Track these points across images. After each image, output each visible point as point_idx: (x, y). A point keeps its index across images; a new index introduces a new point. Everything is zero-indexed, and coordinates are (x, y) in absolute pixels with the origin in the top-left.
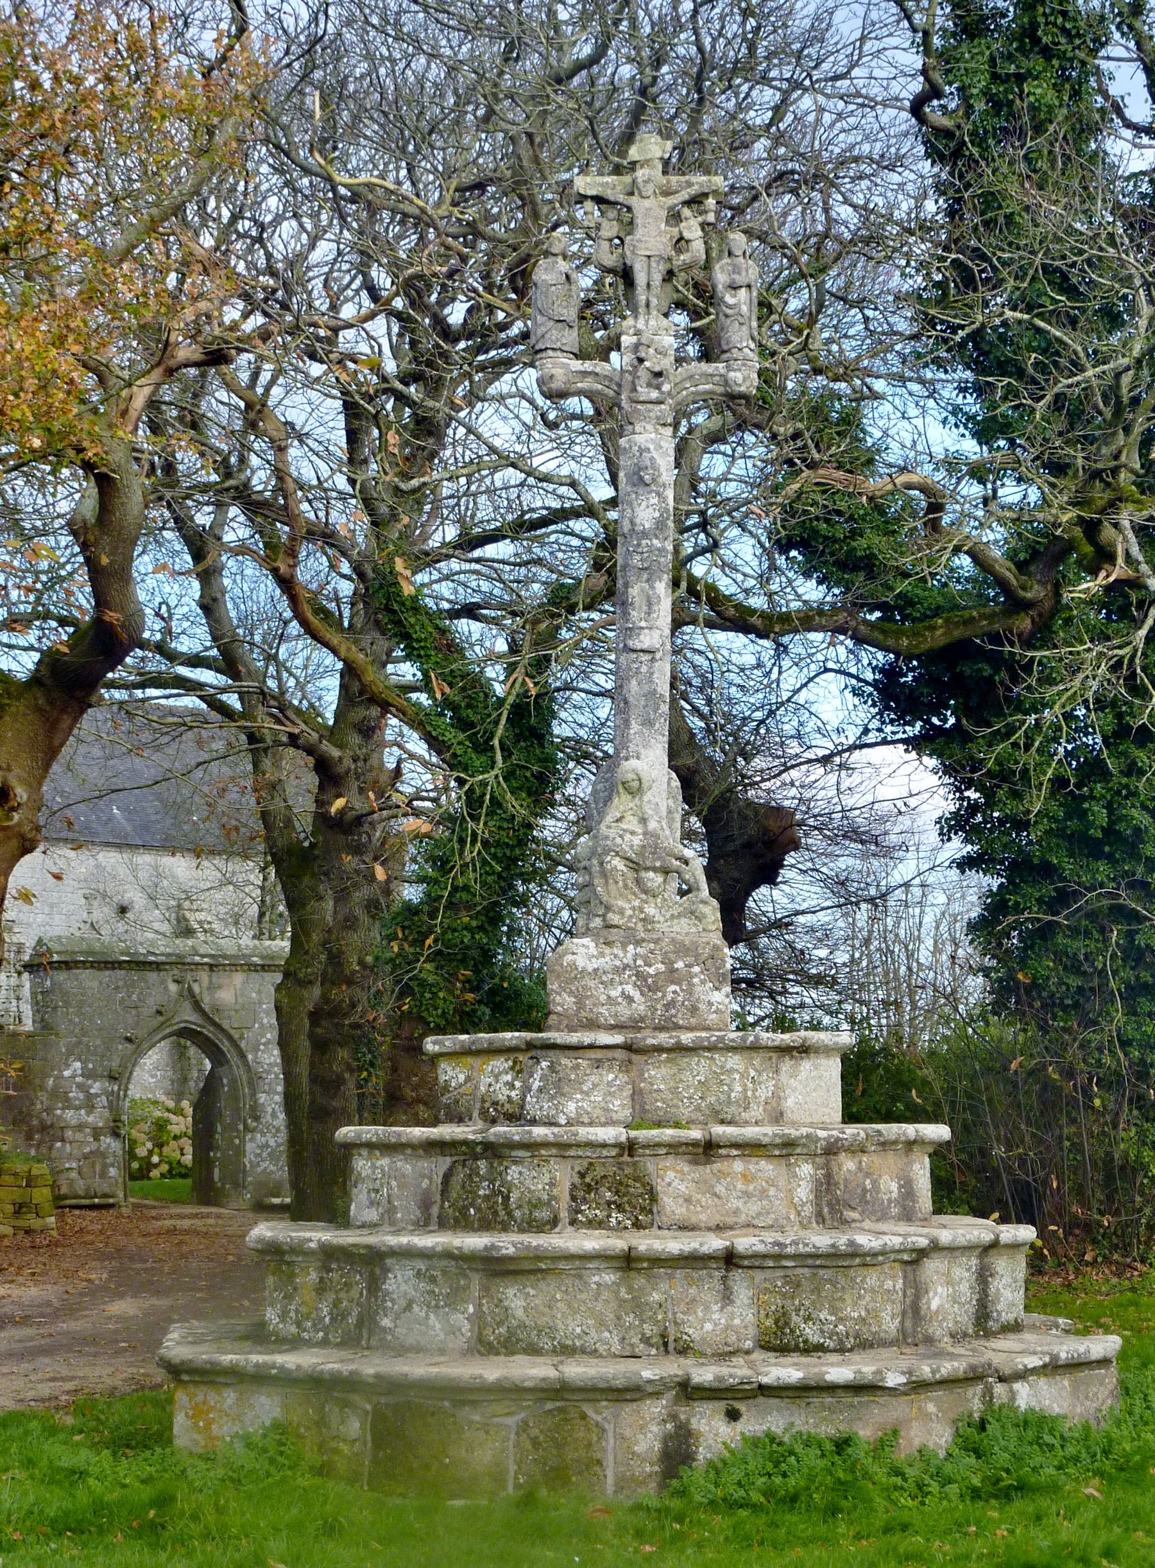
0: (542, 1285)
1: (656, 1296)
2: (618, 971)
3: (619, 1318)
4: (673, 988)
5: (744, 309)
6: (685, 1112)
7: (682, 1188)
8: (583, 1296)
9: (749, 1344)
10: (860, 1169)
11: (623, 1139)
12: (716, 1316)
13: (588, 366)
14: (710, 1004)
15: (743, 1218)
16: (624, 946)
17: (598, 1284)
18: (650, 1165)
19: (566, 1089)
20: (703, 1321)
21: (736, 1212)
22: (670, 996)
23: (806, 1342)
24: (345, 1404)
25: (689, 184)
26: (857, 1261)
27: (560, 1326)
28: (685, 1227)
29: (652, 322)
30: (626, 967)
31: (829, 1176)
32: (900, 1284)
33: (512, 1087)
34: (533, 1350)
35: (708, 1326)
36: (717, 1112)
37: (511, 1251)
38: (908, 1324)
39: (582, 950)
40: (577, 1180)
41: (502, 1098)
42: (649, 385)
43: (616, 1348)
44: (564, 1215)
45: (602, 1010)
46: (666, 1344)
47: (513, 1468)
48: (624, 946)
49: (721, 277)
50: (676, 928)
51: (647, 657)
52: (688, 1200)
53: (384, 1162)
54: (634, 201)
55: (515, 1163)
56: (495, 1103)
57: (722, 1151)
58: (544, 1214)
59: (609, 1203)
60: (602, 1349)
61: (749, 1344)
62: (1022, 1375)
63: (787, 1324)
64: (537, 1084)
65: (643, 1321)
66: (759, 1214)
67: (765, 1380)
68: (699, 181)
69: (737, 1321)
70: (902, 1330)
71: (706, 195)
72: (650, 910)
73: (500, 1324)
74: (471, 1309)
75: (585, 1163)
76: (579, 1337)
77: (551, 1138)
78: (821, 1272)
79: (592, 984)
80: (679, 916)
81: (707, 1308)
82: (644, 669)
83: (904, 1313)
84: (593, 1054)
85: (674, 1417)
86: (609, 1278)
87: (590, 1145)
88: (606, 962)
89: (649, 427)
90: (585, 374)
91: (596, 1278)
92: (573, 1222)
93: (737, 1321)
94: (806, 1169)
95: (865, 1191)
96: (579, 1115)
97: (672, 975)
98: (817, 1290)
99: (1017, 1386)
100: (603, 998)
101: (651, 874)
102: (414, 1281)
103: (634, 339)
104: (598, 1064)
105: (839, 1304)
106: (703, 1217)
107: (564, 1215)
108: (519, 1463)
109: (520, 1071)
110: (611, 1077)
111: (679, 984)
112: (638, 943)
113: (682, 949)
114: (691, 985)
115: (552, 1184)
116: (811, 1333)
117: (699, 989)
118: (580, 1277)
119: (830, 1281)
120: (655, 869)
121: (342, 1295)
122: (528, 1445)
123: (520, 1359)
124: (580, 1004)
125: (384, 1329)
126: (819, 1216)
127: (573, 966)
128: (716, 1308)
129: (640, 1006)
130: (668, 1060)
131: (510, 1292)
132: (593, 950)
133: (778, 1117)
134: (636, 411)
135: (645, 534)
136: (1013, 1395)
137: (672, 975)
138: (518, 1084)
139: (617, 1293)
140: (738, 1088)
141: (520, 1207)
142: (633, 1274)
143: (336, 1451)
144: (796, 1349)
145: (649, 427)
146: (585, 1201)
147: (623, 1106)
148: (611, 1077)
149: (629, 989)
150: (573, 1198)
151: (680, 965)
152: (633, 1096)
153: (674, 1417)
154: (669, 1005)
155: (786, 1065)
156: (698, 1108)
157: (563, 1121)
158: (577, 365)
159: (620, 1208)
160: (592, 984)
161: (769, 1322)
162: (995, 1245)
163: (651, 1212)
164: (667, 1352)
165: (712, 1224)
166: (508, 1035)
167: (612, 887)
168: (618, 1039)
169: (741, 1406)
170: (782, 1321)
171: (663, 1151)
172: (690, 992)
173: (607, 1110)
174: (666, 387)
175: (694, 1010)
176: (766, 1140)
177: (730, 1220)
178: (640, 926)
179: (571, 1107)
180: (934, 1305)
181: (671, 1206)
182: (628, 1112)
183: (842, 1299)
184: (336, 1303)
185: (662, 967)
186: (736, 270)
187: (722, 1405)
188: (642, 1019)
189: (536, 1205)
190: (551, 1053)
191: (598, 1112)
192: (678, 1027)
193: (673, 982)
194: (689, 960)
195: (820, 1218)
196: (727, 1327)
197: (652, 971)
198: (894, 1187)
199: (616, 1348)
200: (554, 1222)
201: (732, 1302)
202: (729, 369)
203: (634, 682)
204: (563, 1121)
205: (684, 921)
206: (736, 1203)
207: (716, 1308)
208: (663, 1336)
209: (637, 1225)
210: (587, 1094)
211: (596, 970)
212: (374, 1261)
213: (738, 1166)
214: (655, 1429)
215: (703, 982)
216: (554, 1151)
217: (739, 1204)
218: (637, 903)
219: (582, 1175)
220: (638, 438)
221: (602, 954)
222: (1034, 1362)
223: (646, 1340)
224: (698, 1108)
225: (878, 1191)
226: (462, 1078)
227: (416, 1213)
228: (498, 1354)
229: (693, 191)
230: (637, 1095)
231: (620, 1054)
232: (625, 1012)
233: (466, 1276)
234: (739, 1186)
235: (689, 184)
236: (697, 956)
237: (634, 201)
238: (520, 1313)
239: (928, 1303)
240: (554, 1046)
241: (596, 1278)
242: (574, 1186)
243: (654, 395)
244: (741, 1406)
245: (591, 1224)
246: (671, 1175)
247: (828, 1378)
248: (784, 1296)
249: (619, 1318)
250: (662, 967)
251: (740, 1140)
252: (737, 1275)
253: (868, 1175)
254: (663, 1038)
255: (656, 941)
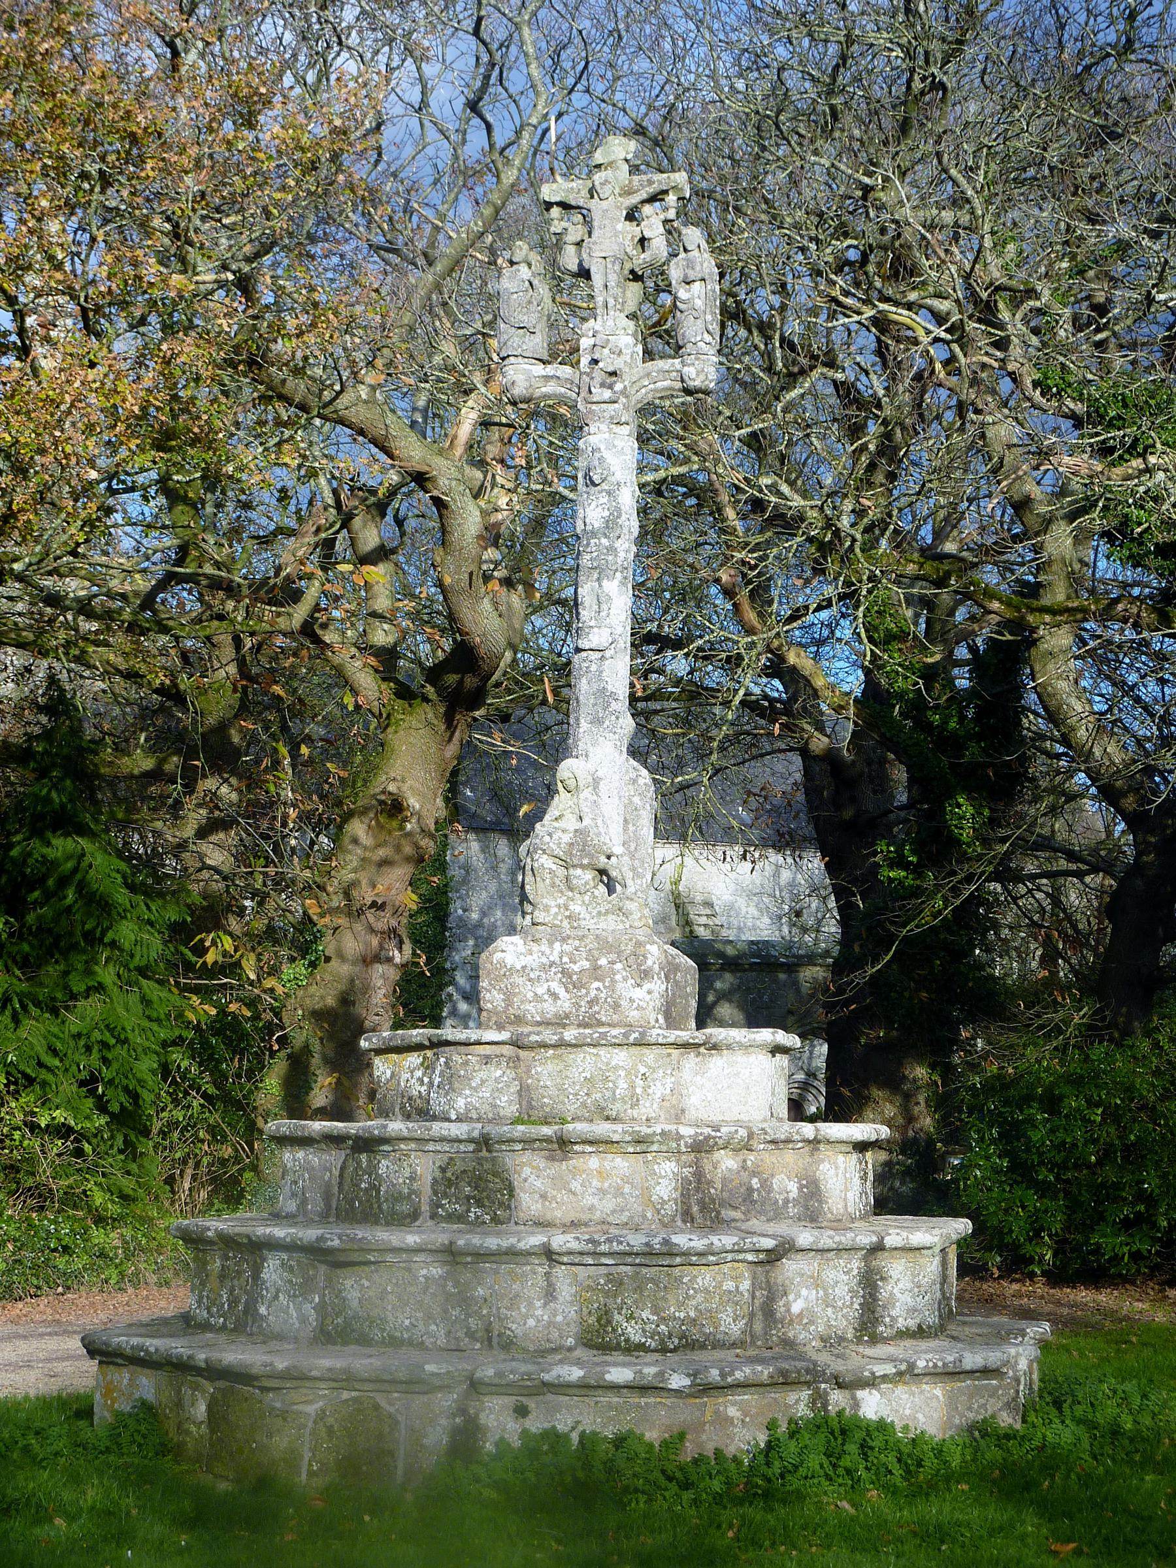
0: (376, 1277)
1: (480, 1291)
2: (544, 968)
3: (446, 1311)
4: (596, 984)
5: (699, 303)
6: (571, 1108)
7: (538, 1184)
8: (412, 1289)
9: (571, 1341)
10: (744, 1168)
11: (476, 1134)
12: (539, 1312)
13: (550, 370)
14: (632, 1000)
15: (597, 1215)
16: (551, 943)
17: (426, 1278)
18: (509, 1160)
19: (456, 1085)
20: (526, 1317)
21: (592, 1208)
22: (593, 993)
23: (627, 1341)
24: (196, 1387)
25: (650, 182)
26: (678, 1260)
27: (390, 1317)
28: (541, 1224)
29: (610, 323)
30: (552, 964)
31: (699, 1175)
32: (746, 1285)
33: (422, 1083)
34: (364, 1340)
35: (531, 1322)
36: (603, 1109)
37: (336, 1243)
38: (758, 1327)
39: (511, 948)
40: (438, 1174)
41: (415, 1093)
42: (602, 385)
43: (442, 1341)
44: (425, 1208)
45: (530, 1007)
46: (490, 1339)
47: (307, 1455)
48: (551, 943)
49: (675, 273)
50: (602, 926)
51: (598, 655)
52: (544, 1197)
53: (300, 1154)
54: (594, 204)
55: (385, 1157)
56: (410, 1098)
57: (577, 1148)
58: (405, 1208)
59: (468, 1198)
60: (428, 1342)
61: (571, 1341)
62: (871, 1382)
63: (609, 1322)
64: (437, 1080)
65: (468, 1315)
66: (614, 1211)
67: (546, 1377)
68: (660, 180)
69: (559, 1318)
70: (749, 1329)
71: (666, 192)
72: (576, 907)
73: (337, 1315)
74: (317, 1300)
75: (445, 1157)
76: (407, 1329)
77: (405, 1133)
78: (644, 1270)
79: (520, 981)
80: (607, 912)
81: (530, 1304)
82: (594, 668)
83: (752, 1315)
84: (480, 1049)
85: (463, 1411)
86: (436, 1271)
87: (442, 1139)
88: (532, 961)
89: (604, 427)
90: (547, 378)
91: (424, 1272)
92: (434, 1216)
93: (559, 1318)
94: (668, 1167)
95: (750, 1190)
96: (468, 1110)
97: (596, 972)
98: (639, 1289)
99: (860, 1394)
100: (530, 995)
101: (579, 871)
102: (280, 1271)
103: (592, 341)
104: (487, 1060)
105: (661, 1304)
106: (558, 1214)
107: (425, 1208)
108: (313, 1451)
109: (427, 1068)
110: (499, 1073)
111: (603, 981)
112: (564, 940)
113: (606, 945)
114: (613, 981)
115: (412, 1178)
116: (633, 1332)
117: (620, 986)
118: (409, 1270)
119: (652, 1280)
120: (582, 867)
121: (236, 1282)
122: (323, 1433)
123: (879, 1346)
124: (508, 1001)
125: (262, 1316)
126: (687, 1216)
127: (503, 963)
128: (538, 1304)
129: (565, 1003)
130: (554, 1057)
131: (348, 1283)
132: (521, 948)
133: (679, 1115)
134: (591, 412)
135: (593, 534)
136: (856, 1405)
137: (596, 972)
138: (426, 1080)
139: (445, 1286)
140: (622, 1084)
141: (386, 1200)
142: (460, 1268)
143: (188, 1432)
144: (618, 1347)
145: (604, 427)
146: (445, 1195)
147: (510, 1102)
148: (499, 1073)
149: (555, 986)
150: (435, 1193)
151: (603, 962)
152: (519, 1092)
153: (463, 1411)
154: (591, 1003)
155: (691, 1061)
156: (584, 1104)
157: (454, 1117)
158: (539, 370)
159: (479, 1203)
160: (520, 981)
161: (592, 1320)
162: (878, 1248)
163: (509, 1207)
164: (490, 1346)
165: (567, 1220)
166: (415, 1032)
167: (540, 884)
168: (504, 1036)
169: (531, 1403)
170: (605, 1318)
171: (519, 1147)
172: (612, 988)
173: (495, 1106)
174: (618, 387)
175: (616, 1006)
176: (616, 1138)
177: (585, 1217)
178: (565, 923)
179: (461, 1103)
180: (796, 1308)
181: (528, 1203)
182: (515, 1108)
183: (664, 1299)
184: (232, 1290)
185: (587, 965)
186: (690, 264)
187: (510, 1401)
188: (567, 1016)
189: (398, 1198)
190: (447, 1049)
191: (486, 1107)
192: (601, 1024)
193: (597, 979)
194: (613, 956)
195: (687, 1216)
196: (551, 1323)
197: (576, 968)
198: (793, 1188)
199: (442, 1341)
200: (415, 1215)
201: (555, 1298)
202: (683, 364)
203: (584, 681)
204: (454, 1117)
205: (611, 917)
206: (589, 1200)
207: (538, 1304)
208: (488, 1330)
209: (496, 1220)
210: (475, 1089)
211: (524, 968)
212: (257, 1248)
213: (594, 1162)
214: (444, 1422)
215: (625, 979)
216: (413, 1146)
217: (595, 1201)
218: (561, 901)
219: (443, 1170)
220: (592, 439)
221: (530, 952)
222: (889, 1369)
223: (470, 1334)
224: (584, 1104)
225: (770, 1190)
226: (389, 1073)
227: (320, 1206)
228: (334, 1344)
229: (651, 190)
230: (524, 1092)
231: (507, 1050)
232: (550, 1008)
233: (315, 1267)
234: (595, 1183)
235: (650, 182)
236: (619, 953)
237: (594, 204)
238: (355, 1304)
239: (788, 1306)
240: (448, 1043)
241: (424, 1272)
242: (435, 1181)
243: (607, 394)
244: (531, 1403)
245: (452, 1217)
246: (527, 1171)
247: (608, 1377)
248: (607, 1294)
249: (446, 1311)
250: (587, 965)
251: (590, 1137)
252: (560, 1271)
253: (754, 1174)
254: (549, 1036)
255: (582, 938)
